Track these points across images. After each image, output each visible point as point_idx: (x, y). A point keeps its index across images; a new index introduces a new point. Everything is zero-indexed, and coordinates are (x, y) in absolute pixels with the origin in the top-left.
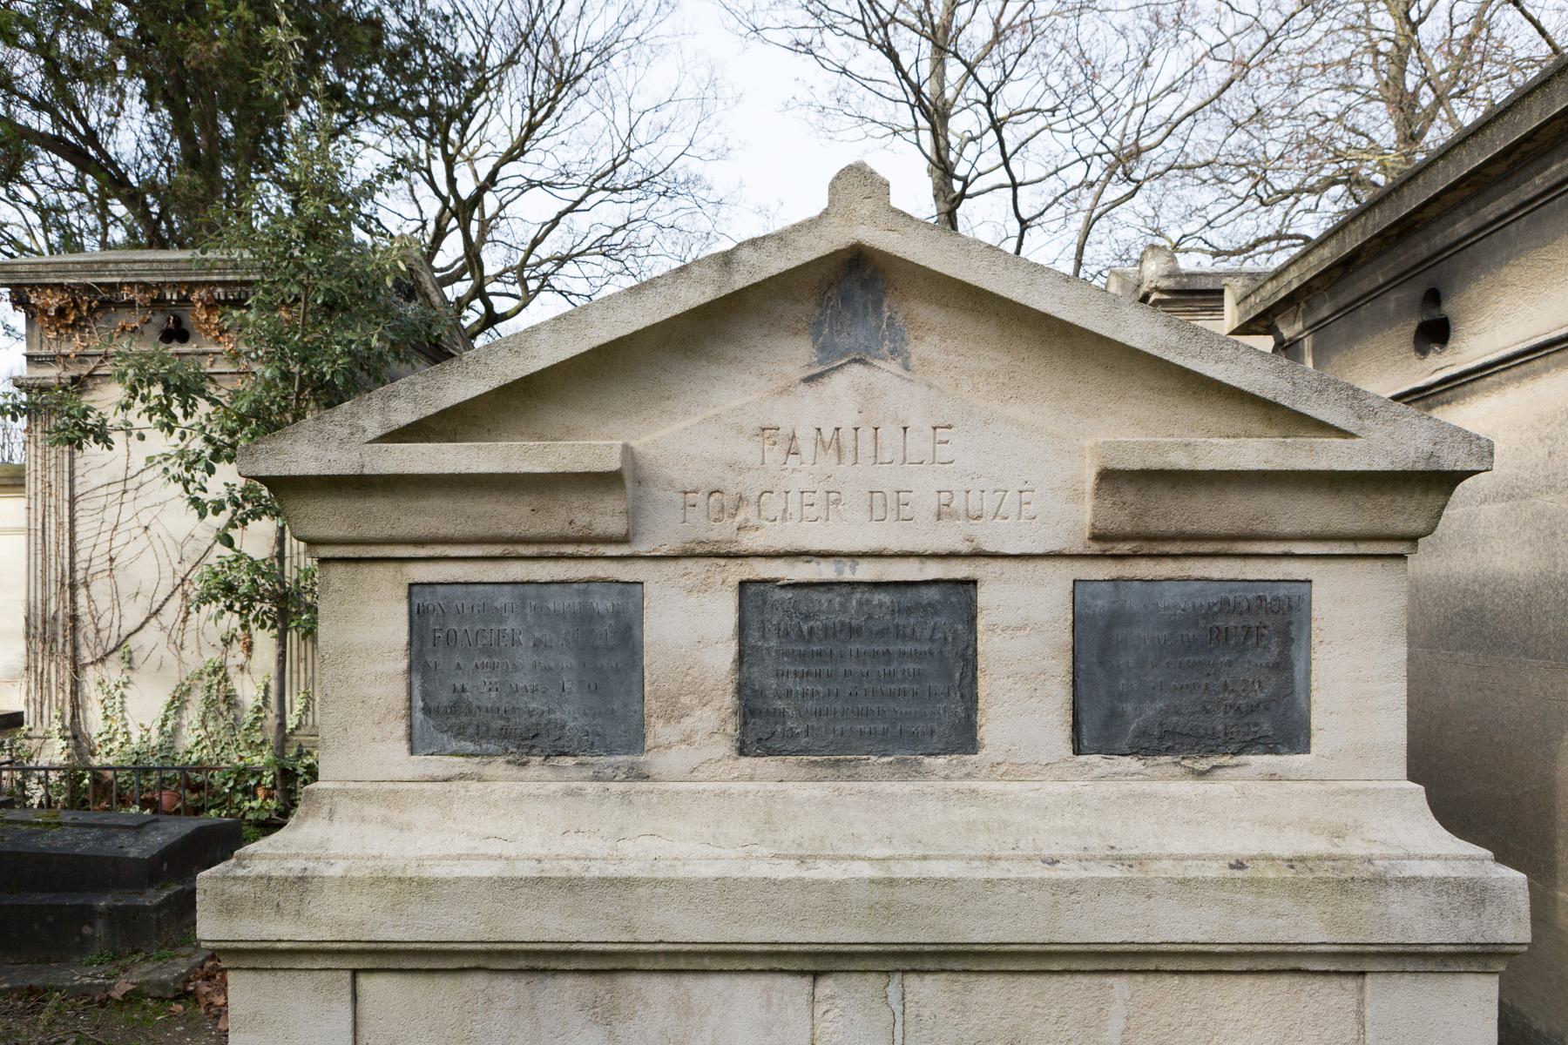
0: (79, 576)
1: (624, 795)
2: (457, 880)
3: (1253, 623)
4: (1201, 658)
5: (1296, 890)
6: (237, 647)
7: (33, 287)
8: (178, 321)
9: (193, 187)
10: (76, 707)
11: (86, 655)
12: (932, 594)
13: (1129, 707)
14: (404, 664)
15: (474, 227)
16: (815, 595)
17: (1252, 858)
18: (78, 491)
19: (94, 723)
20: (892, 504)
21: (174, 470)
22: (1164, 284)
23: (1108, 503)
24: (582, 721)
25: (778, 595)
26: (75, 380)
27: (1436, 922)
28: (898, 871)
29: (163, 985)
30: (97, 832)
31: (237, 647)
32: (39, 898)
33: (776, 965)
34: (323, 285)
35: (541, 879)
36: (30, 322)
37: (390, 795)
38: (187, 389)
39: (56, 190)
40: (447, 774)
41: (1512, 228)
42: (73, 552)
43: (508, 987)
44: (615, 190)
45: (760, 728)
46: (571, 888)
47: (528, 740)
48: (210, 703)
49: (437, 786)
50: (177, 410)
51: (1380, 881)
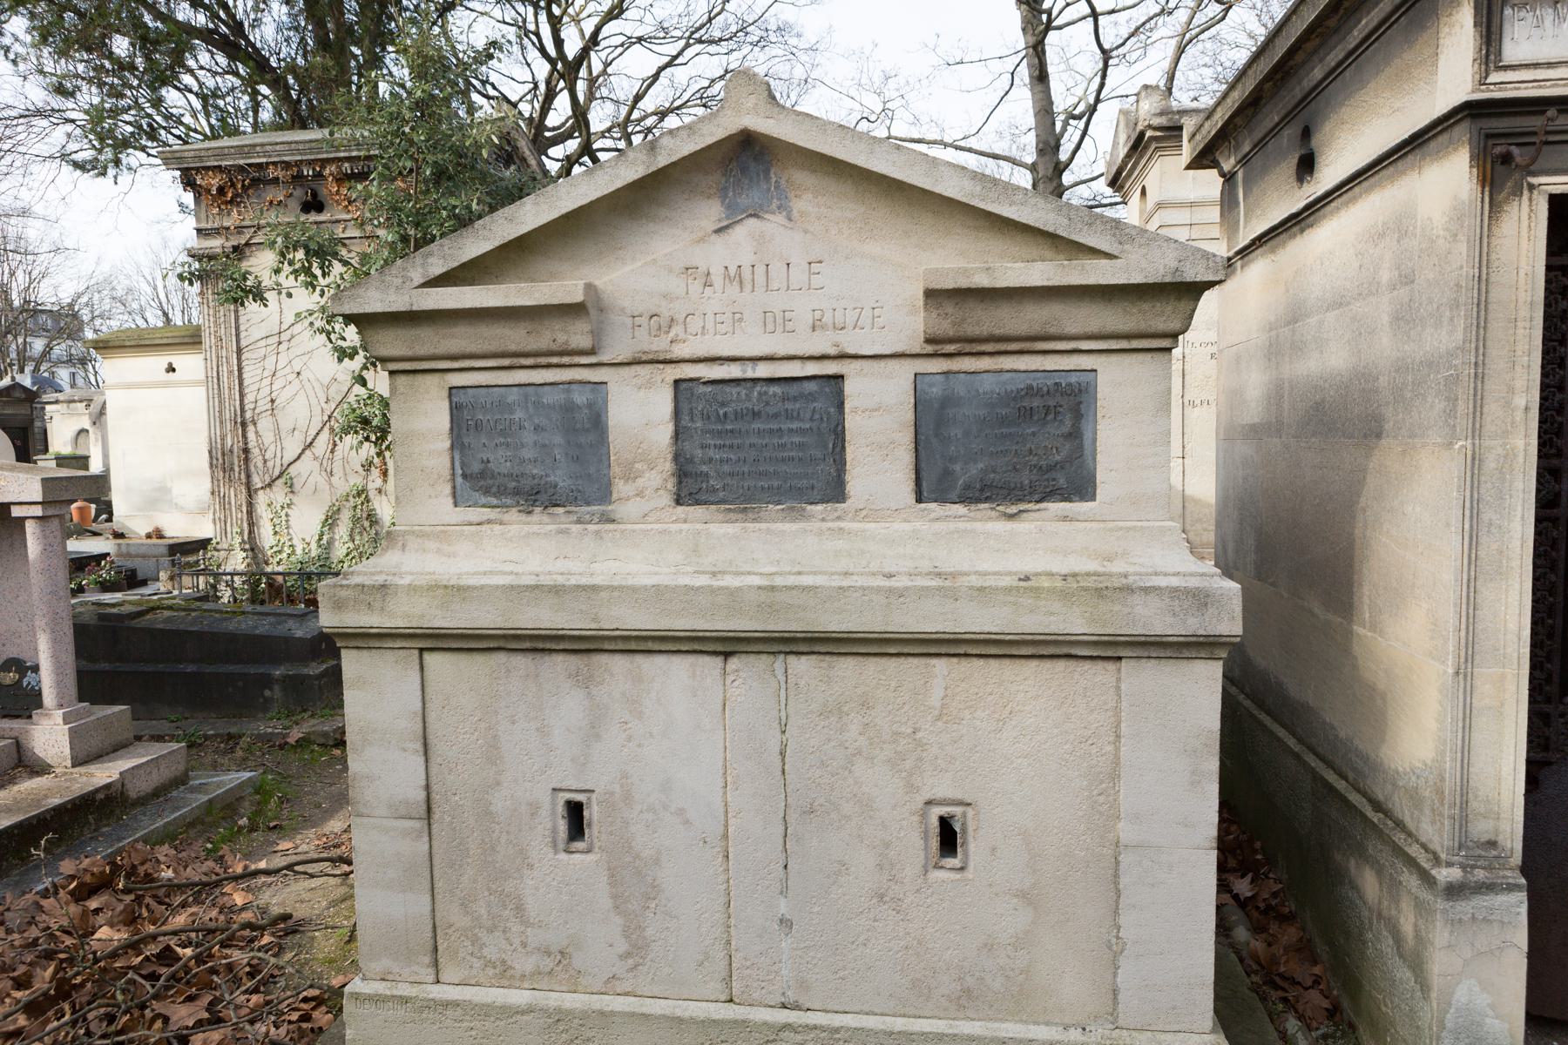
0: (248, 415)
1: (597, 532)
2: (482, 587)
3: (1052, 403)
4: (1012, 430)
5: (1065, 595)
6: (375, 473)
7: (198, 170)
8: (315, 194)
9: (325, 69)
10: (251, 524)
11: (257, 481)
12: (812, 386)
13: (957, 467)
14: (448, 444)
15: (581, 86)
16: (728, 389)
17: (1037, 574)
18: (243, 343)
19: (267, 538)
20: (780, 321)
21: (319, 324)
22: (1156, 121)
23: (934, 315)
24: (569, 482)
25: (702, 389)
26: (236, 249)
27: (1169, 619)
28: (779, 581)
29: (325, 735)
30: (271, 619)
31: (375, 473)
32: (231, 668)
33: (696, 647)
34: (431, 158)
35: (537, 587)
36: (197, 200)
37: (441, 534)
38: (323, 253)
39: (214, 74)
40: (478, 519)
41: (1347, 73)
42: (242, 395)
43: (520, 662)
44: (711, 42)
45: (690, 486)
46: (557, 592)
47: (533, 495)
48: (356, 520)
49: (473, 528)
50: (318, 272)
51: (1129, 590)
